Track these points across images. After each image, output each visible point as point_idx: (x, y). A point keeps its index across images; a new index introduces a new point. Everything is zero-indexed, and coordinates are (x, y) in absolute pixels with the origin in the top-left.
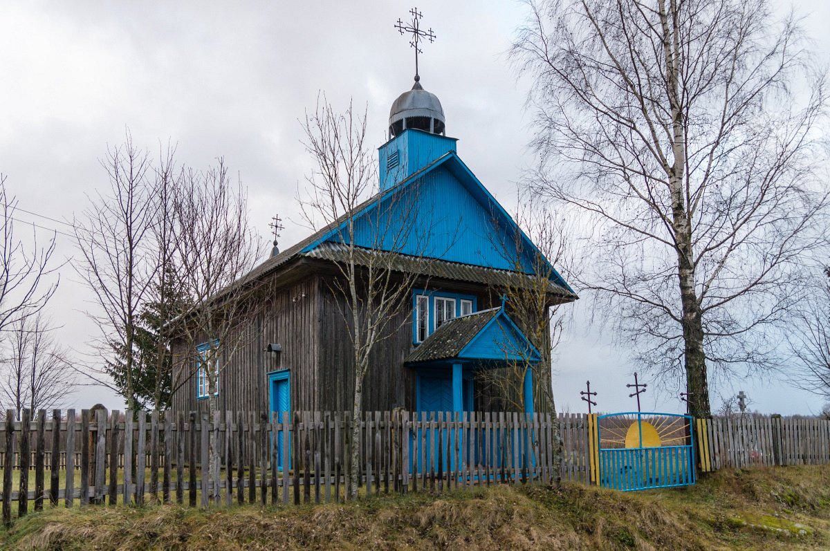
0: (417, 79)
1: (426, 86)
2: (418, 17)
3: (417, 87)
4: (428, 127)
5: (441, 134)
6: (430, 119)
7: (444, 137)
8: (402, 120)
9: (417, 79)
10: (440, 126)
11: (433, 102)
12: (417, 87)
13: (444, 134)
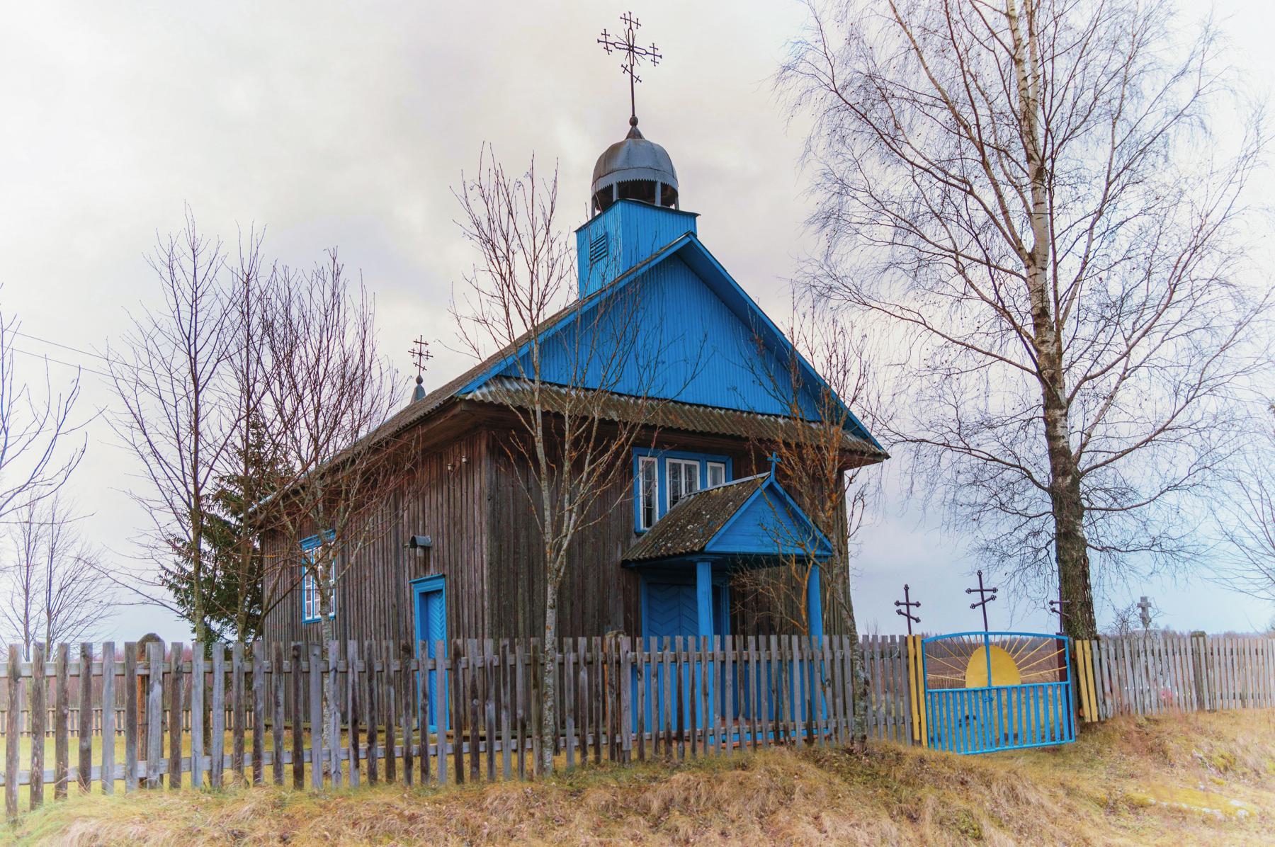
0: (634, 122)
1: (649, 133)
2: (634, 26)
3: (634, 134)
4: (652, 196)
5: (673, 207)
6: (653, 184)
7: (677, 212)
8: (611, 187)
9: (634, 122)
10: (671, 195)
11: (660, 157)
12: (634, 134)
13: (677, 206)
